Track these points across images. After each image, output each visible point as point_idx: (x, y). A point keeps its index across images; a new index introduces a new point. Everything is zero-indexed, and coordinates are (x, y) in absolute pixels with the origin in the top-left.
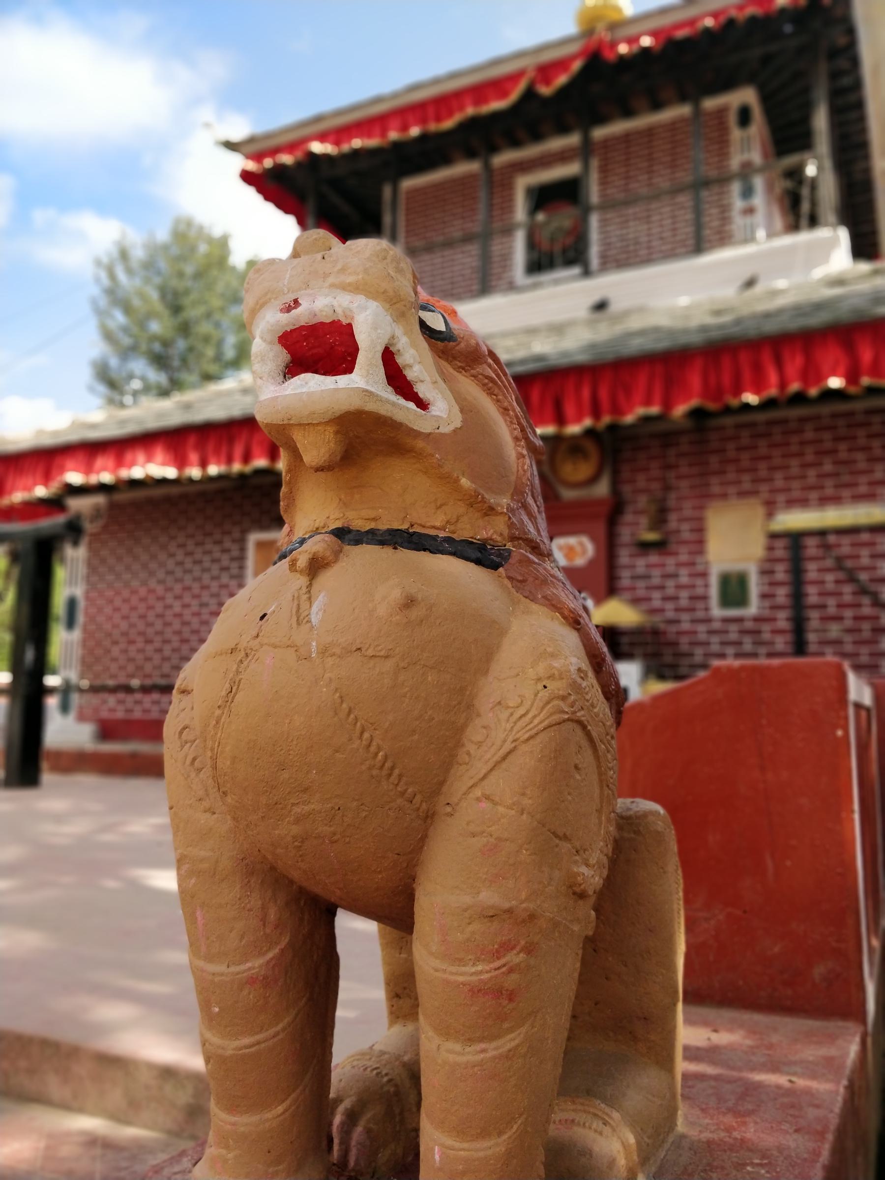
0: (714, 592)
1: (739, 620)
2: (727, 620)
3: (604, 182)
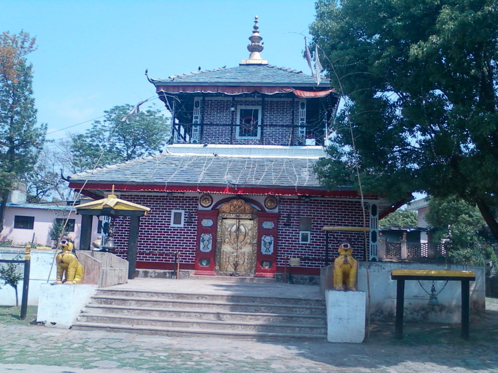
0: (300, 238)
1: (306, 244)
2: (302, 244)
3: (263, 115)
